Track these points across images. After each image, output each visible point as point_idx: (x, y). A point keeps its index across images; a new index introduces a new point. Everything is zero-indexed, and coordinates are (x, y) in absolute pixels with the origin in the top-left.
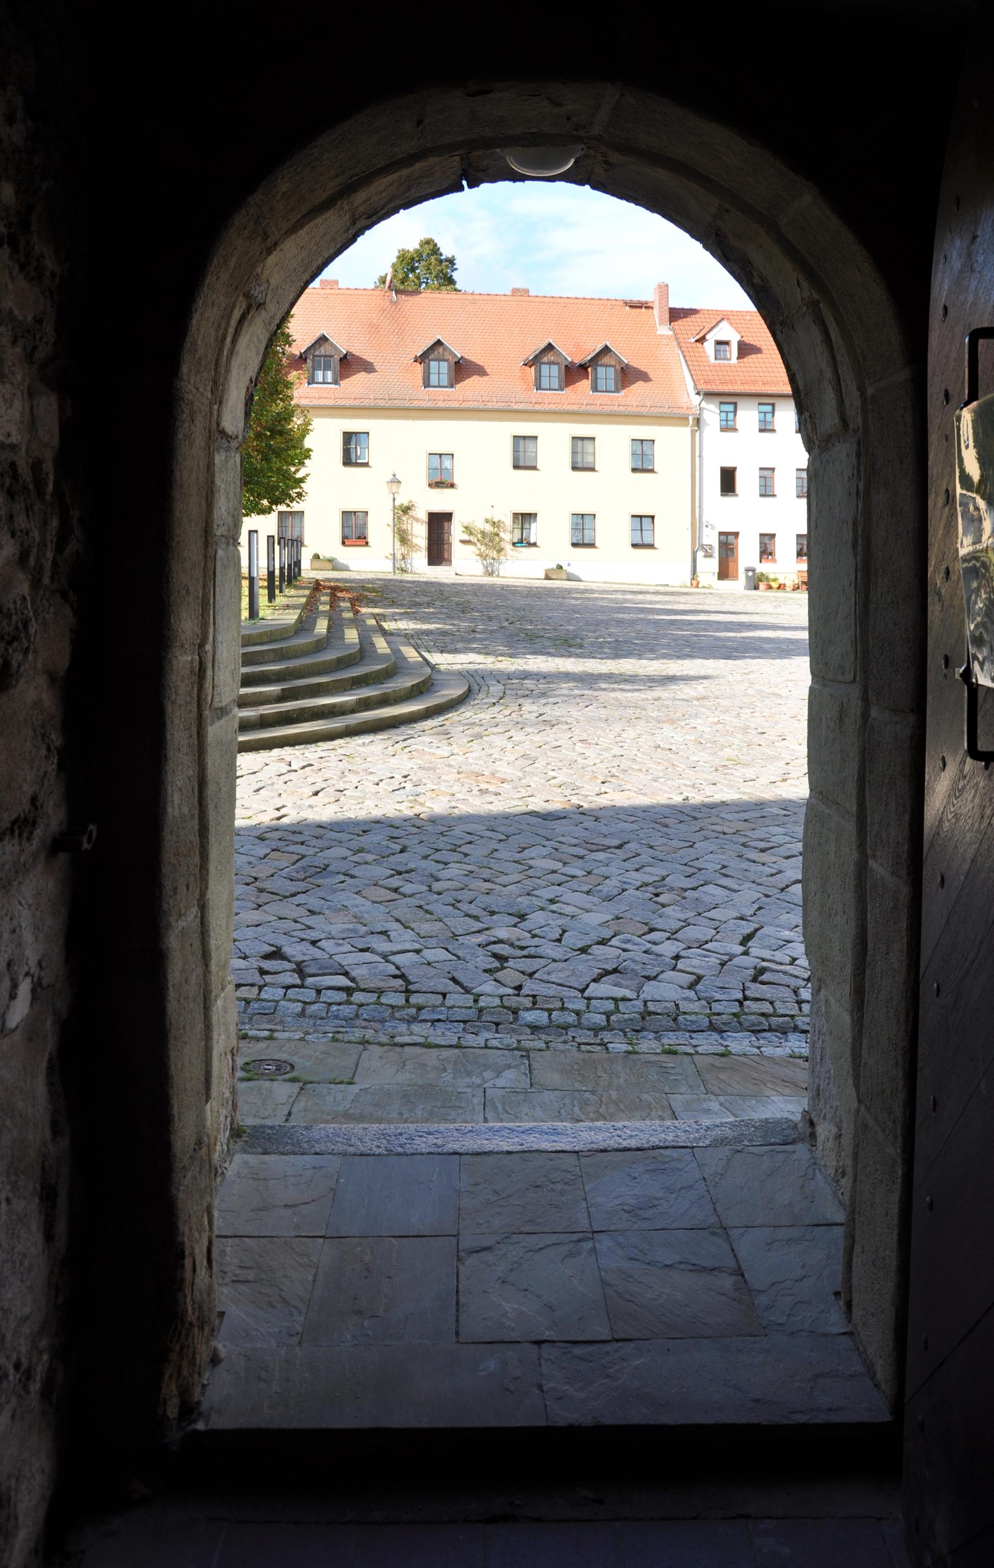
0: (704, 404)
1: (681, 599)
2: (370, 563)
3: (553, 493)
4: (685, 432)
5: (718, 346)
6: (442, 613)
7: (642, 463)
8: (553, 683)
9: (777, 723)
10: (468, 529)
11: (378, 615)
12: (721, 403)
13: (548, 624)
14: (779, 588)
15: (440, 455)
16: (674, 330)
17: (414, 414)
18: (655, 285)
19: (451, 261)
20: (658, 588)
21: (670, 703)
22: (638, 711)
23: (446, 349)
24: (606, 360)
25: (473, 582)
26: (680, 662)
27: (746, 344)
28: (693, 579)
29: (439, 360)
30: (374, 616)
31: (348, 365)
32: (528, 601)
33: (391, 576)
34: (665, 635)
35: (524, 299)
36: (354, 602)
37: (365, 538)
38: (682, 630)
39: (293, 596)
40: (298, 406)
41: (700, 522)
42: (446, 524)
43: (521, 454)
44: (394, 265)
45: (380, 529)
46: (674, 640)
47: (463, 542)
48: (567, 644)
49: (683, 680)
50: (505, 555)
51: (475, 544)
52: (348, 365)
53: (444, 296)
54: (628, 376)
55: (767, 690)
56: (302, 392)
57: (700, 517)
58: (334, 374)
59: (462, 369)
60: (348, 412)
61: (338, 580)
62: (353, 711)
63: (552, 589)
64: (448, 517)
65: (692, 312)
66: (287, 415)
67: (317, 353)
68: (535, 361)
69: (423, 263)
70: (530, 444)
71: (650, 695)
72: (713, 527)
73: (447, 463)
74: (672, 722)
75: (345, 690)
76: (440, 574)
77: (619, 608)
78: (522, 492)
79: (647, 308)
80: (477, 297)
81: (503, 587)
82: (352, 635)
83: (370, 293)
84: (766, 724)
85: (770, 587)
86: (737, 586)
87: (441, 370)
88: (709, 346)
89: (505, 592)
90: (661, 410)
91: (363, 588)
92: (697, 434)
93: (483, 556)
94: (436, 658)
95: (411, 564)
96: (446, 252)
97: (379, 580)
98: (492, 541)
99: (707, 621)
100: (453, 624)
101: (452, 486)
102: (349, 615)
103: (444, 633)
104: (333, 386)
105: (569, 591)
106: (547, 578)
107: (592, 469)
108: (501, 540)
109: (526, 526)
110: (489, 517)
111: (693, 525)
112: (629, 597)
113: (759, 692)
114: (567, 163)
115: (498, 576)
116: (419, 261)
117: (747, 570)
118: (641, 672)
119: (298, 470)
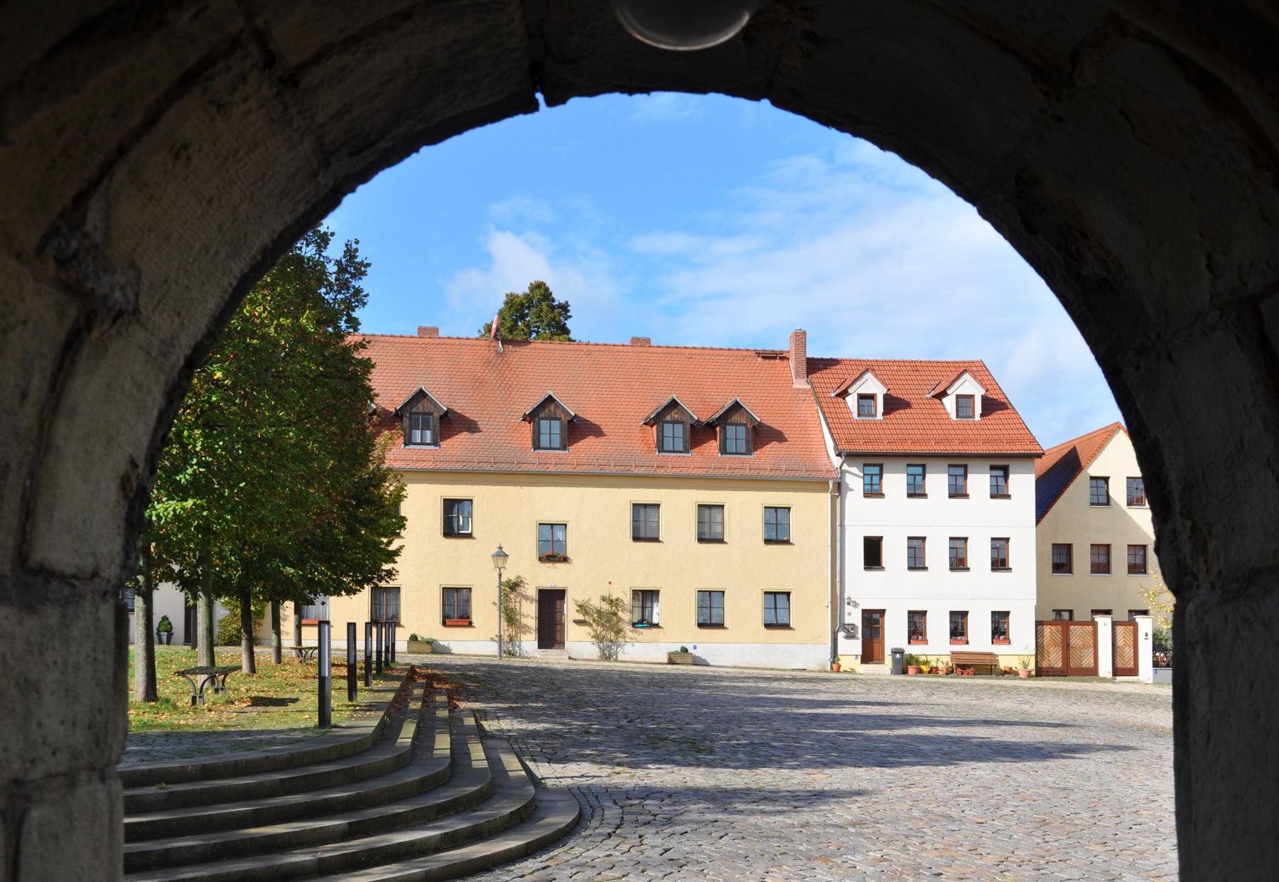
0: (845, 467)
1: (821, 687)
2: (474, 645)
3: (678, 567)
4: (826, 498)
5: (862, 401)
6: (551, 708)
7: (777, 531)
8: (680, 803)
9: (953, 859)
10: (582, 608)
11: (478, 711)
12: (865, 465)
13: (672, 722)
14: (930, 672)
15: (552, 525)
16: (811, 383)
17: (524, 479)
18: (791, 333)
19: (564, 308)
20: (794, 673)
21: (821, 831)
22: (783, 843)
23: (558, 406)
24: (736, 418)
25: (588, 668)
26: (827, 771)
27: (894, 398)
28: (833, 662)
29: (550, 418)
30: (474, 713)
31: (450, 424)
32: (651, 691)
33: (496, 661)
34: (808, 735)
35: (645, 349)
36: (451, 695)
37: (468, 617)
38: (827, 728)
39: (382, 691)
40: (390, 470)
41: (842, 598)
42: (558, 602)
43: (642, 524)
44: (501, 312)
45: (484, 609)
46: (820, 741)
47: (577, 622)
48: (695, 750)
49: (834, 797)
50: (624, 637)
51: (590, 625)
52: (450, 424)
53: (556, 346)
54: (761, 435)
55: (935, 810)
56: (394, 452)
57: (842, 592)
58: (434, 435)
59: (576, 429)
60: (449, 477)
61: (436, 666)
62: (437, 850)
63: (676, 676)
64: (560, 594)
65: (833, 362)
66: (379, 478)
67: (414, 410)
68: (657, 420)
69: (534, 310)
70: (651, 511)
71: (795, 819)
72: (856, 605)
73: (559, 535)
74: (825, 858)
75: (429, 821)
76: (553, 659)
77: (752, 699)
79: (782, 358)
80: (592, 348)
81: (622, 674)
82: (443, 743)
83: (474, 342)
84: (941, 861)
85: (920, 671)
86: (884, 669)
87: (552, 430)
88: (852, 401)
89: (625, 681)
90: (798, 474)
91: (465, 676)
92: (838, 500)
93: (599, 638)
94: (543, 770)
95: (519, 646)
96: (559, 297)
97: (483, 665)
98: (609, 621)
99: (853, 715)
100: (563, 724)
101: (565, 560)
102: (442, 713)
103: (552, 735)
104: (432, 447)
105: (695, 678)
106: (671, 662)
107: (721, 541)
108: (620, 620)
109: (649, 604)
110: (606, 595)
112: (763, 685)
113: (926, 812)
114: (739, 17)
115: (616, 660)
116: (528, 308)
117: (894, 652)
118: (783, 786)
119: (390, 543)
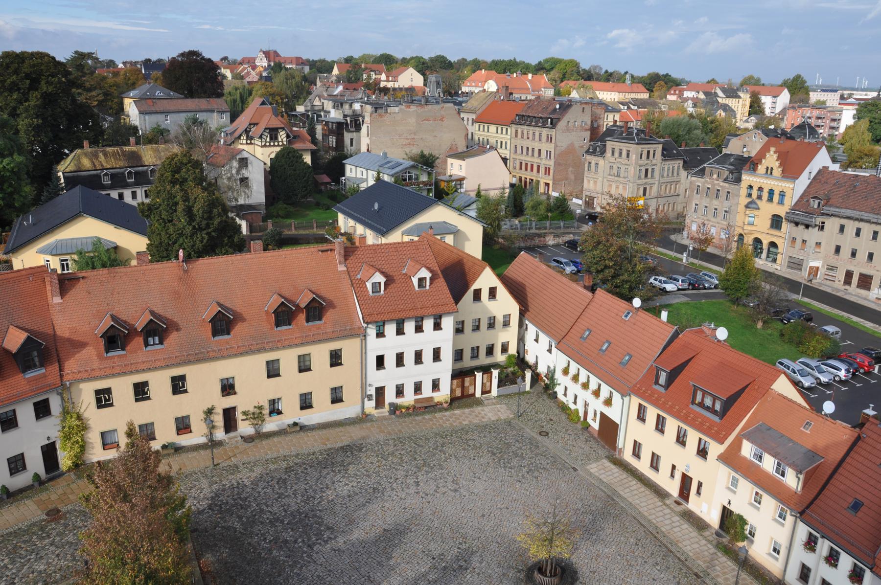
3: (290, 385)
7: (336, 359)
64: (234, 408)
78: (271, 388)
111: (362, 387)
